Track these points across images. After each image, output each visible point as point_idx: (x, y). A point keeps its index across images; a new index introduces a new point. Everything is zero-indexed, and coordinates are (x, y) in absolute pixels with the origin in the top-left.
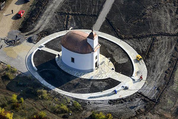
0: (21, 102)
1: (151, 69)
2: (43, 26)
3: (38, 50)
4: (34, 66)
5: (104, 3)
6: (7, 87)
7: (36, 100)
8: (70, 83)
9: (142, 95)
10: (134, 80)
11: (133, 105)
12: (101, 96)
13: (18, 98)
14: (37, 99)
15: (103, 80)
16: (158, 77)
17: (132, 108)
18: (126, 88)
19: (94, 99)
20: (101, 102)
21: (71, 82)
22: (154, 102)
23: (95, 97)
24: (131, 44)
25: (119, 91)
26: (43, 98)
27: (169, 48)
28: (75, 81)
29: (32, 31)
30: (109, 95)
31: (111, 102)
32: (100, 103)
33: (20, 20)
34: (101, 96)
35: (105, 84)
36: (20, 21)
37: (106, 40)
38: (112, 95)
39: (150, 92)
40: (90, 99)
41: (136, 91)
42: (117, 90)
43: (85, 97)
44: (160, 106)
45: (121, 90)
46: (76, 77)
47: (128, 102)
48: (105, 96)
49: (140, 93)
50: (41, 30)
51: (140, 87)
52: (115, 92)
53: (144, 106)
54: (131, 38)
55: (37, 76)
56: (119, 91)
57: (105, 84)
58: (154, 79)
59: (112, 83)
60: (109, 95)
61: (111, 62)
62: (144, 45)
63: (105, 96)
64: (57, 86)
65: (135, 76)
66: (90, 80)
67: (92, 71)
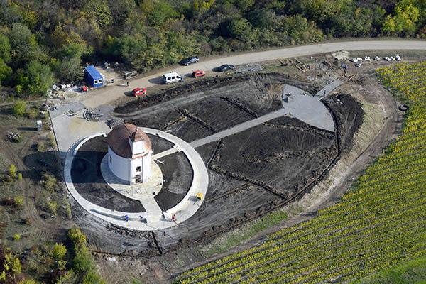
0: (17, 178)
1: (200, 214)
2: (142, 115)
3: (103, 135)
4: (77, 149)
5: (241, 123)
6: (25, 157)
7: (36, 184)
8: (91, 185)
9: (154, 237)
10: (163, 216)
11: (130, 242)
12: (106, 215)
13: (17, 173)
14: (37, 184)
15: (128, 199)
16: (198, 227)
17: (126, 244)
18: (145, 221)
19: (96, 214)
20: (100, 221)
21: (93, 184)
22: (160, 251)
23: (98, 213)
24: (212, 179)
25: (130, 219)
26: (44, 186)
27: (253, 204)
28: (98, 185)
29: (122, 115)
30: (116, 218)
31: (113, 227)
32: (97, 222)
33: (193, 79)
34: (106, 215)
35: (127, 204)
36: (131, 99)
37: (188, 160)
38: (121, 220)
39: (163, 242)
40: (91, 212)
41: (152, 229)
42: (129, 217)
43: (88, 206)
44: (161, 259)
45: (136, 219)
46: (105, 182)
47: (129, 236)
48: (111, 216)
49: (153, 234)
50: (134, 118)
51: (162, 228)
52: (126, 219)
53: (142, 249)
54: (220, 173)
55: (68, 163)
56: (130, 219)
57: (127, 204)
58: (190, 228)
59: (136, 207)
60: (116, 218)
61: (161, 186)
62: (224, 186)
63: (111, 216)
64: (74, 181)
65: (170, 213)
66: (115, 192)
67: (128, 183)
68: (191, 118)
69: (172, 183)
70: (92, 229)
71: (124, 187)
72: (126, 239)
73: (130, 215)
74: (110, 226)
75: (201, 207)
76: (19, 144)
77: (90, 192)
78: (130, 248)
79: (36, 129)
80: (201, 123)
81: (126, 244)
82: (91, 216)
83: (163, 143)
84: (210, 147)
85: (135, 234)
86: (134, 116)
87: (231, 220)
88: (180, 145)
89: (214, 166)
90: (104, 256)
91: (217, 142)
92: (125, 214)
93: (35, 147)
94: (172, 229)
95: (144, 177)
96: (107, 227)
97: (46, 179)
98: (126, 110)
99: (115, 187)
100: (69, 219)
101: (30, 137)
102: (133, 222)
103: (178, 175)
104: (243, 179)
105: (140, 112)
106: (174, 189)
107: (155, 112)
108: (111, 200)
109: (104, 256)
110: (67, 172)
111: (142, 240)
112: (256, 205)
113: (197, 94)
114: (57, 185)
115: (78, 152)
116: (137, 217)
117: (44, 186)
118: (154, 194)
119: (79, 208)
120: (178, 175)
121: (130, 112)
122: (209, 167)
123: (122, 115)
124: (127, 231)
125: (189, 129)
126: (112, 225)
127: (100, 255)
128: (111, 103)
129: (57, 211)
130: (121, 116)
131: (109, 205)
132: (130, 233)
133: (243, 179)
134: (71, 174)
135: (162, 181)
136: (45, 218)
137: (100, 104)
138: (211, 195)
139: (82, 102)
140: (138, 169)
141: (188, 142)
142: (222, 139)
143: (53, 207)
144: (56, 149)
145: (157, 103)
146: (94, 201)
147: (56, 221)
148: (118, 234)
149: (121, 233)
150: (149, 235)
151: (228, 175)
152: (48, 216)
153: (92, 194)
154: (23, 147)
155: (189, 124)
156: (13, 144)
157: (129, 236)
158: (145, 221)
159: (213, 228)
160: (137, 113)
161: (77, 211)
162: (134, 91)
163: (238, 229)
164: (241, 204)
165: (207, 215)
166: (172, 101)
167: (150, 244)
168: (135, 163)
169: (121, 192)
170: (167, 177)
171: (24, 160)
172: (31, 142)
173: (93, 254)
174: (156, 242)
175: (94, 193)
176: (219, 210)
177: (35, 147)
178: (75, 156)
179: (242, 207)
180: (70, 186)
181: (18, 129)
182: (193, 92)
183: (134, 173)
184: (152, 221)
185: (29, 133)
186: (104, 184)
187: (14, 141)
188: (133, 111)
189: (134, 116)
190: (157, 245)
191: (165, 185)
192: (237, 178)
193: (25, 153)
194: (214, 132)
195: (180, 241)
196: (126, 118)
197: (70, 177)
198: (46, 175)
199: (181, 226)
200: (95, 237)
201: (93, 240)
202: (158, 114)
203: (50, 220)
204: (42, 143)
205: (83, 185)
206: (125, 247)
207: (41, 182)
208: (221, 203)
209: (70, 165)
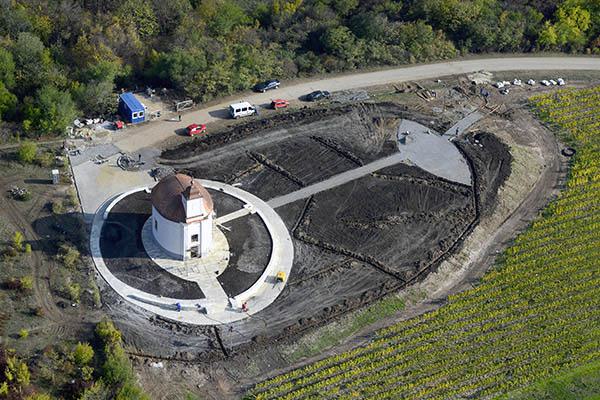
0: (24, 251)
1: (281, 302)
2: (201, 163)
3: (145, 191)
4: (108, 210)
5: (340, 173)
6: (35, 222)
7: (50, 259)
8: (128, 261)
9: (217, 334)
10: (230, 304)
11: (184, 341)
12: (150, 303)
13: (24, 243)
14: (52, 259)
15: (180, 281)
16: (279, 320)
17: (177, 344)
18: (204, 311)
19: (135, 302)
20: (141, 312)
21: (131, 259)
22: (225, 354)
23: (139, 299)
24: (298, 253)
25: (183, 309)
26: (62, 262)
27: (356, 288)
28: (138, 261)
29: (173, 161)
30: (164, 307)
31: (159, 320)
32: (137, 313)
33: (272, 111)
34: (150, 303)
35: (179, 288)
36: (184, 139)
37: (265, 225)
38: (171, 309)
39: (230, 341)
40: (129, 299)
41: (215, 323)
42: (182, 305)
43: (124, 290)
44: (227, 364)
45: (191, 309)
46: (148, 256)
47: (181, 333)
48: (157, 305)
49: (216, 329)
50: (189, 166)
51: (228, 321)
52: (178, 308)
53: (201, 350)
54: (311, 244)
55: (96, 229)
56: (183, 309)
57: (179, 288)
58: (268, 321)
59: (192, 291)
60: (164, 307)
61: (227, 262)
62: (315, 262)
63: (157, 305)
64: (105, 255)
65: (239, 300)
66: (162, 270)
67: (181, 258)
68: (269, 166)
69: (242, 258)
70: (130, 323)
71: (174, 263)
72: (177, 336)
73: (183, 303)
74: (154, 318)
75: (283, 291)
76: (27, 202)
77: (127, 270)
78: (183, 350)
79: (51, 182)
80: (282, 173)
81: (177, 344)
82: (129, 305)
83: (229, 202)
84: (296, 208)
85: (190, 329)
86: (189, 163)
87: (326, 309)
88: (253, 204)
89: (301, 234)
90: (146, 361)
91: (306, 199)
92: (176, 301)
93: (49, 207)
94: (243, 322)
95: (203, 250)
96: (151, 320)
97: (65, 252)
98: (177, 155)
99: (161, 263)
100: (98, 309)
101: (43, 193)
102: (188, 313)
103: (251, 246)
104: (342, 253)
105: (197, 157)
106: (246, 266)
107: (218, 158)
108: (156, 282)
109: (146, 361)
110: (95, 243)
111: (200, 339)
112: (360, 289)
113: (277, 133)
114: (80, 261)
115: (110, 214)
116: (193, 305)
117: (62, 262)
118: (217, 273)
119: (111, 293)
120: (251, 246)
121: (183, 158)
122: (295, 236)
123: (173, 161)
124: (179, 325)
125: (266, 182)
126: (158, 317)
127: (141, 359)
128: (156, 145)
129: (80, 298)
130: (170, 164)
131: (154, 288)
132: (183, 328)
133: (342, 253)
134: (100, 246)
135: (228, 254)
136: (63, 307)
137: (141, 146)
138: (297, 274)
139: (115, 144)
140: (195, 237)
141: (265, 200)
142: (313, 196)
143: (75, 291)
144: (79, 210)
145: (221, 146)
146: (132, 283)
147: (80, 311)
148: (166, 330)
149: (171, 328)
150: (210, 331)
151: (321, 246)
152: (67, 305)
153: (130, 274)
154: (33, 208)
155: (266, 174)
156: (19, 202)
157: (181, 333)
158: (204, 311)
159: (300, 321)
160: (193, 159)
161: (109, 297)
162: (189, 129)
163: (335, 323)
164: (339, 287)
165: (291, 303)
166: (242, 143)
167: (211, 344)
168: (190, 229)
169: (170, 271)
170: (236, 250)
171: (34, 225)
172: (44, 200)
173: (131, 358)
174: (220, 341)
175: (132, 271)
176: (309, 296)
177: (49, 207)
178: (106, 220)
179: (341, 292)
180: (99, 262)
181: (26, 182)
182: (272, 129)
183: (189, 244)
184: (213, 311)
185: (41, 187)
186: (147, 260)
187: (20, 198)
188: (187, 157)
189: (189, 163)
190: (221, 345)
191: (233, 260)
192: (333, 251)
193: (35, 216)
194: (301, 186)
195: (254, 339)
196: (178, 167)
197: (99, 249)
198: (64, 247)
199: (254, 318)
200: (134, 334)
201: (131, 337)
202: (223, 161)
203: (70, 310)
204: (59, 202)
205: (117, 261)
206: (175, 348)
207: (58, 256)
208: (312, 285)
209: (99, 233)
